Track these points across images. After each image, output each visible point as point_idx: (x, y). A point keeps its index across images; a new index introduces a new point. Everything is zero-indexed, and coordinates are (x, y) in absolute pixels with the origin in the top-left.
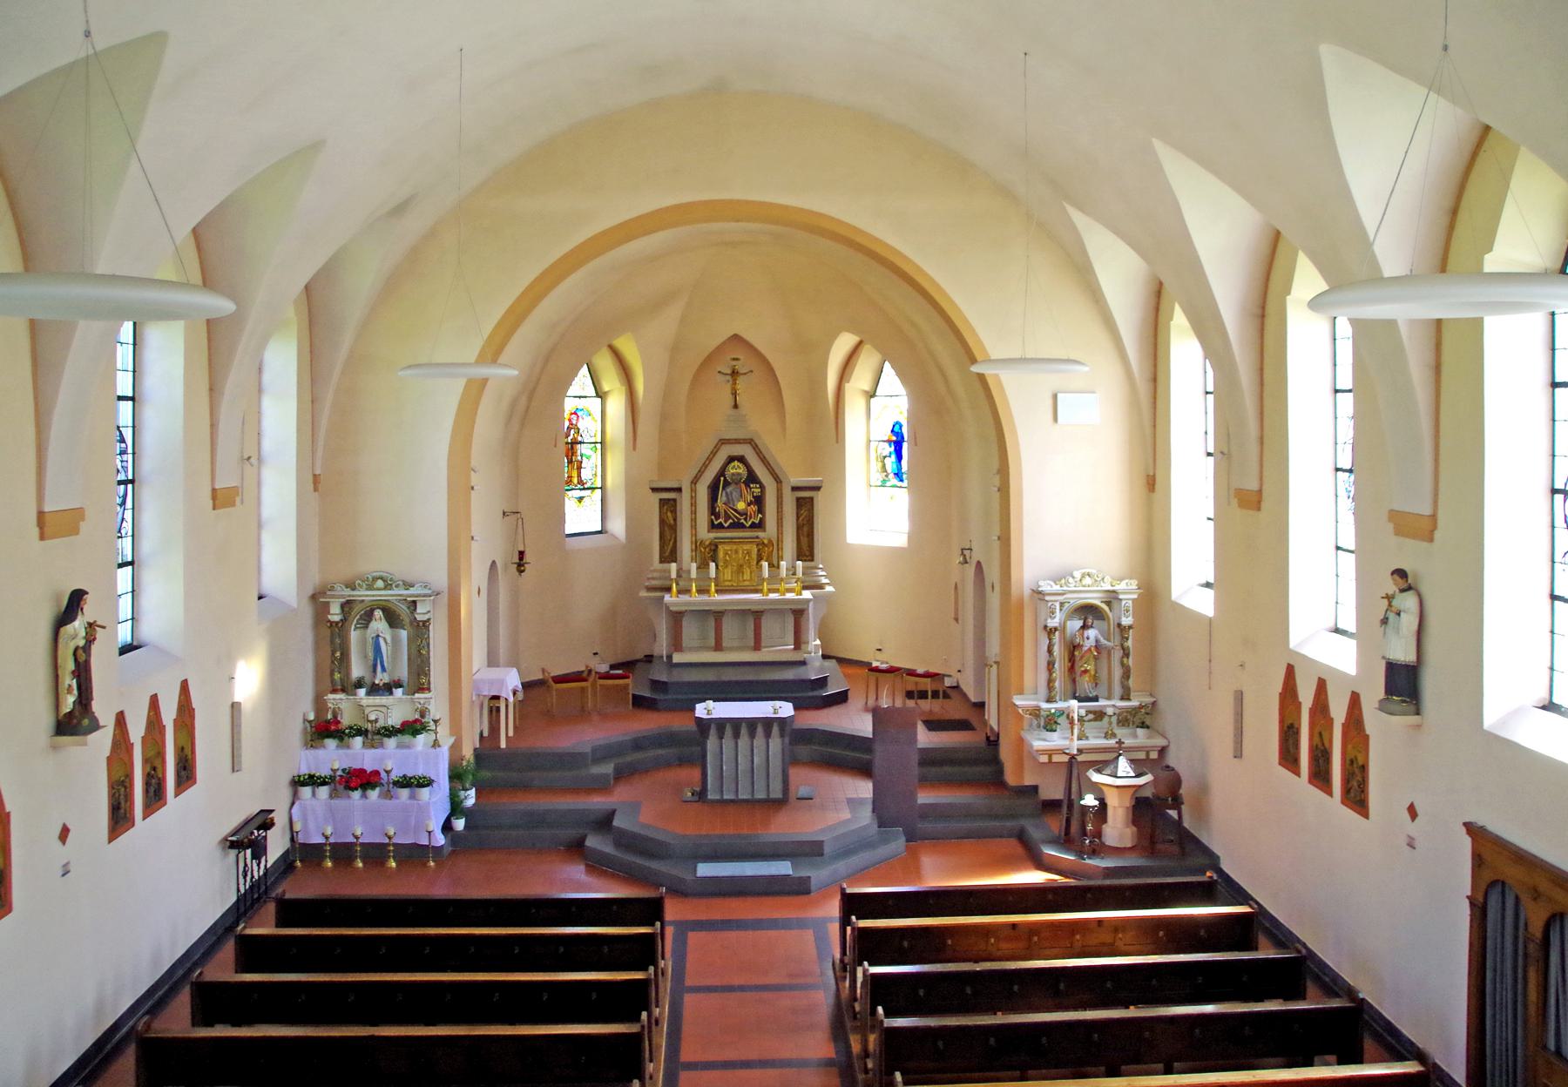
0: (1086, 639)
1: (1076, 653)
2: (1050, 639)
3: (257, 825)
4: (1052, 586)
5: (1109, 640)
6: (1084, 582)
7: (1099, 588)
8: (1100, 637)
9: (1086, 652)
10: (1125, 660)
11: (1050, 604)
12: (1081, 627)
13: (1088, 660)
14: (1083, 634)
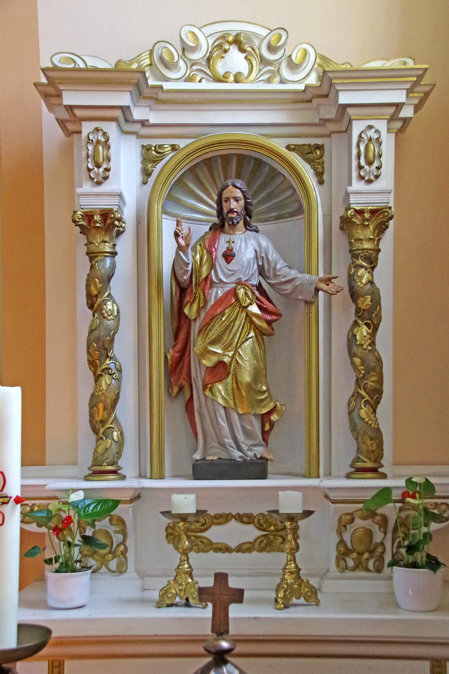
7: (275, 86)
9: (220, 301)
13: (228, 328)
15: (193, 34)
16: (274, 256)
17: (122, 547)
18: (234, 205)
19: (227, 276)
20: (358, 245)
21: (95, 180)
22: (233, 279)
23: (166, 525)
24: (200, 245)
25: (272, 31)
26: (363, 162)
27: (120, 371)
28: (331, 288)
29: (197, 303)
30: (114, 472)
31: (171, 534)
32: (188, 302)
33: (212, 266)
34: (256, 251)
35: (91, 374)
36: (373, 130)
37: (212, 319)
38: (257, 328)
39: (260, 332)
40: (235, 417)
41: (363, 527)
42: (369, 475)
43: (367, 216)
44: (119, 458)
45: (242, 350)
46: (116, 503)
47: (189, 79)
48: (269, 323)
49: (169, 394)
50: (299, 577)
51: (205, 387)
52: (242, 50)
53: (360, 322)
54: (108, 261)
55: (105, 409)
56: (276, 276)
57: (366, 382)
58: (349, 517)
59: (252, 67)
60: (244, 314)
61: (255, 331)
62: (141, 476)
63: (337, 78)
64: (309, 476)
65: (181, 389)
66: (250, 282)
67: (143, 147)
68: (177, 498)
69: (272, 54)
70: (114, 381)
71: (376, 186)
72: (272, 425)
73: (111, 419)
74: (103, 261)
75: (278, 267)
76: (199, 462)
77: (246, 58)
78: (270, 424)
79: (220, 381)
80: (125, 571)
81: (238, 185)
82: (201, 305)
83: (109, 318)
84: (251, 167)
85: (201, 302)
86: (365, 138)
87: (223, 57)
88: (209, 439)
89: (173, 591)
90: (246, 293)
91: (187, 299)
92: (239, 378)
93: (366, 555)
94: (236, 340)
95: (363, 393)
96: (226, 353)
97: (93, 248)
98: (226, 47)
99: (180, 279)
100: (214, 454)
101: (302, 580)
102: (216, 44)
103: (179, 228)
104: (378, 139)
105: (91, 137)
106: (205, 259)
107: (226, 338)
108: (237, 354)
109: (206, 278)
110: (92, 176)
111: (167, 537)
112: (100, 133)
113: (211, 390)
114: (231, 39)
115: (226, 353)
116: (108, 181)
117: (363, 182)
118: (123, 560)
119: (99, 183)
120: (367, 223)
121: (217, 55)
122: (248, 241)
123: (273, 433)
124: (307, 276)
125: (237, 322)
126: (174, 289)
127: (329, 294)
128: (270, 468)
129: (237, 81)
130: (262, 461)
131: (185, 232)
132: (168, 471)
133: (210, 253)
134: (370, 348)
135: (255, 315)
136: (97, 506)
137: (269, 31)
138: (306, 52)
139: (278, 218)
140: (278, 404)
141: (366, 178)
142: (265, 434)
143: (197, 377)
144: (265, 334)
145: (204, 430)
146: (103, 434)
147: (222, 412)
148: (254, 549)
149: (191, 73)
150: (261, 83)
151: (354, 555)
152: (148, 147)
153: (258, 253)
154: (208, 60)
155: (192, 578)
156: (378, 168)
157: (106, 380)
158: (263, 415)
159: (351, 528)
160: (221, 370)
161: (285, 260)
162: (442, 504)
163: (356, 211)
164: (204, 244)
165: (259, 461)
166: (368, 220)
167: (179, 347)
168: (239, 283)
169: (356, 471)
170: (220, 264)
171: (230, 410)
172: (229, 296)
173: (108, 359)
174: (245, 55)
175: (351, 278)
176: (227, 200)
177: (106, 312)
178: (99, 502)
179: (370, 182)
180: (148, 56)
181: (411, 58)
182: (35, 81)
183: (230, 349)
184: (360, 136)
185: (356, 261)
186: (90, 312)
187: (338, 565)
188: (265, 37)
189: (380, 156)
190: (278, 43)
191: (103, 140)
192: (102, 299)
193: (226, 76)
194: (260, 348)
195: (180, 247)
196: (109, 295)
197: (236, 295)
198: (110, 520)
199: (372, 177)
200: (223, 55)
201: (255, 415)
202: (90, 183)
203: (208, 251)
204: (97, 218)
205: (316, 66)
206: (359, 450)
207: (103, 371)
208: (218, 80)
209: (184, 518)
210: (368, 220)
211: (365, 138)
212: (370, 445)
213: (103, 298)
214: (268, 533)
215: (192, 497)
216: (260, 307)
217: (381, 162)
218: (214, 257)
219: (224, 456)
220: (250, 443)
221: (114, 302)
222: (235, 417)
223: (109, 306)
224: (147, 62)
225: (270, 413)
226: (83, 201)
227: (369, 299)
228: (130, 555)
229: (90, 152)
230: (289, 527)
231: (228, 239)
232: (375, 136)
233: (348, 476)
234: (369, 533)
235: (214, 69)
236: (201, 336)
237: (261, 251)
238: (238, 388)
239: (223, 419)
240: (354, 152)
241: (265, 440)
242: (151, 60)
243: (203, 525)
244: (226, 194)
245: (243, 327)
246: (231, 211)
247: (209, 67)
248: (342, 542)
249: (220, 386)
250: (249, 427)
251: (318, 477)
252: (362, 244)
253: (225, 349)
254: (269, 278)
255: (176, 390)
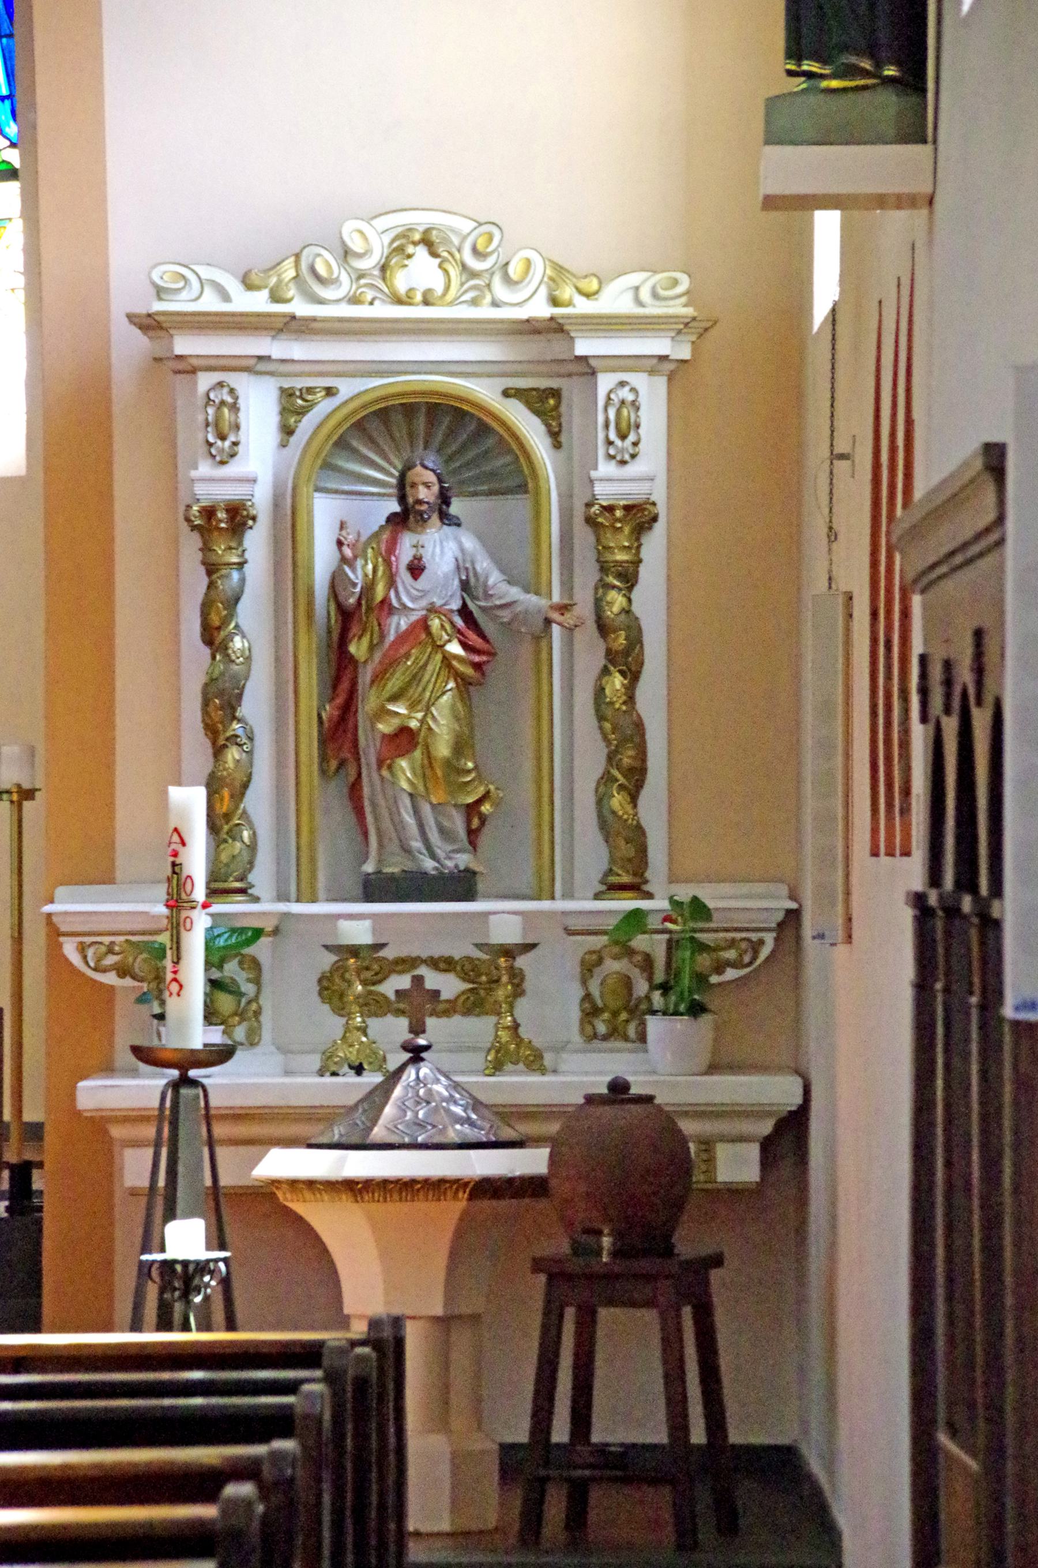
0: (404, 576)
1: (357, 649)
2: (212, 569)
3: (213, 1299)
4: (226, 297)
5: (533, 587)
6: (401, 281)
7: (485, 312)
8: (484, 564)
9: (403, 638)
10: (616, 600)
11: (205, 381)
12: (392, 519)
13: (415, 678)
14: (392, 546)
15: (361, 232)
16: (485, 565)
17: (254, 1006)
18: (423, 493)
19: (414, 599)
20: (609, 557)
21: (218, 458)
22: (424, 603)
23: (319, 976)
24: (373, 548)
25: (480, 224)
26: (613, 436)
27: (251, 739)
28: (569, 619)
29: (368, 637)
30: (243, 891)
31: (327, 989)
32: (354, 636)
33: (391, 582)
34: (457, 560)
35: (208, 743)
36: (627, 389)
37: (391, 665)
38: (458, 676)
39: (465, 684)
40: (426, 810)
41: (618, 973)
42: (629, 894)
43: (619, 513)
44: (250, 870)
45: (437, 709)
46: (258, 933)
47: (355, 300)
48: (478, 666)
49: (323, 772)
50: (517, 1036)
51: (380, 764)
52: (434, 254)
53: (612, 668)
54: (235, 575)
55: (232, 796)
56: (488, 596)
57: (620, 756)
58: (594, 957)
59: (449, 281)
60: (439, 657)
61: (456, 680)
62: (282, 897)
63: (576, 330)
64: (539, 898)
65: (342, 764)
66: (447, 607)
67: (282, 390)
68: (344, 925)
69: (478, 260)
70: (244, 754)
71: (633, 469)
72: (483, 819)
73: (240, 811)
74: (228, 576)
75: (491, 582)
76: (373, 877)
77: (440, 266)
78: (480, 818)
79: (402, 755)
80: (257, 1044)
81: (430, 465)
82: (375, 642)
83: (238, 661)
84: (446, 421)
85: (375, 636)
86: (616, 400)
87: (406, 266)
88: (386, 841)
89: (341, 1054)
90: (442, 626)
91: (355, 630)
92: (434, 753)
93: (624, 1016)
94: (428, 694)
95: (615, 772)
96: (413, 715)
97: (213, 558)
98: (410, 249)
99: (341, 598)
100: (394, 865)
101: (522, 1040)
102: (395, 245)
103: (344, 533)
104: (633, 402)
105: (212, 396)
106: (380, 573)
107: (414, 692)
108: (430, 715)
109: (382, 602)
110: (213, 451)
111: (320, 994)
112: (225, 390)
113: (390, 767)
114: (417, 237)
115: (413, 715)
116: (236, 458)
117: (613, 462)
118: (255, 1024)
119: (222, 463)
120: (619, 525)
121: (396, 263)
122: (445, 544)
123: (486, 830)
124: (533, 598)
125: (430, 668)
126: (333, 613)
127: (570, 631)
128: (481, 887)
129: (426, 302)
130: (468, 875)
131: (351, 538)
132: (321, 893)
133: (388, 563)
134: (624, 708)
135: (456, 657)
136: (230, 936)
137: (475, 224)
138: (528, 263)
139: (490, 493)
140: (492, 787)
141: (619, 458)
142: (472, 834)
143: (368, 746)
144: (470, 684)
145: (379, 830)
146: (227, 833)
147: (407, 801)
148: (455, 1012)
149: (357, 289)
150: (464, 306)
151: (606, 1015)
152: (290, 391)
153: (460, 562)
154: (384, 268)
155: (366, 1035)
156: (635, 444)
157: (233, 754)
158: (468, 806)
159: (599, 973)
160: (404, 738)
161: (502, 571)
162: (744, 939)
163: (602, 507)
164: (379, 548)
165: (462, 875)
166: (619, 520)
167: (340, 701)
168: (432, 609)
169: (609, 889)
170: (403, 582)
171: (419, 798)
172: (417, 630)
173: (235, 722)
174: (438, 261)
175: (598, 605)
176: (414, 485)
177: (234, 652)
178: (233, 930)
179: (623, 463)
180: (293, 265)
181: (684, 272)
182: (128, 311)
183: (419, 708)
184: (609, 398)
185: (605, 578)
186: (207, 651)
187: (582, 1031)
188: (469, 234)
189: (638, 426)
190: (487, 247)
191: (229, 399)
192: (226, 633)
193: (410, 295)
194: (464, 704)
195: (344, 560)
196: (237, 626)
197: (427, 629)
198: (240, 963)
199: (627, 457)
200: (406, 262)
201: (455, 806)
202: (210, 461)
203: (384, 560)
204: (221, 515)
205: (546, 279)
206: (612, 860)
207: (227, 739)
208: (399, 301)
209: (354, 951)
210: (619, 520)
211: (616, 400)
212: (629, 851)
213: (227, 630)
214: (475, 986)
215: (367, 923)
216: (464, 645)
217: (638, 434)
218: (394, 570)
219: (409, 866)
220: (450, 848)
221: (244, 636)
222: (426, 810)
223: (238, 643)
224: (292, 273)
225: (479, 802)
226: (200, 490)
227: (623, 637)
228: (266, 1018)
229: (210, 418)
230: (504, 965)
231: (415, 542)
232: (630, 397)
233: (597, 896)
234: (627, 983)
235: (392, 285)
236: (374, 688)
237: (464, 561)
238: (430, 763)
239: (408, 813)
240: (601, 419)
241: (473, 843)
242: (297, 271)
243: (376, 974)
244: (411, 476)
245: (438, 675)
246: (420, 502)
247: (384, 279)
248: (588, 997)
249: (403, 763)
250: (446, 824)
251: (553, 898)
252: (613, 553)
253: (412, 707)
254: (477, 599)
255: (334, 764)
